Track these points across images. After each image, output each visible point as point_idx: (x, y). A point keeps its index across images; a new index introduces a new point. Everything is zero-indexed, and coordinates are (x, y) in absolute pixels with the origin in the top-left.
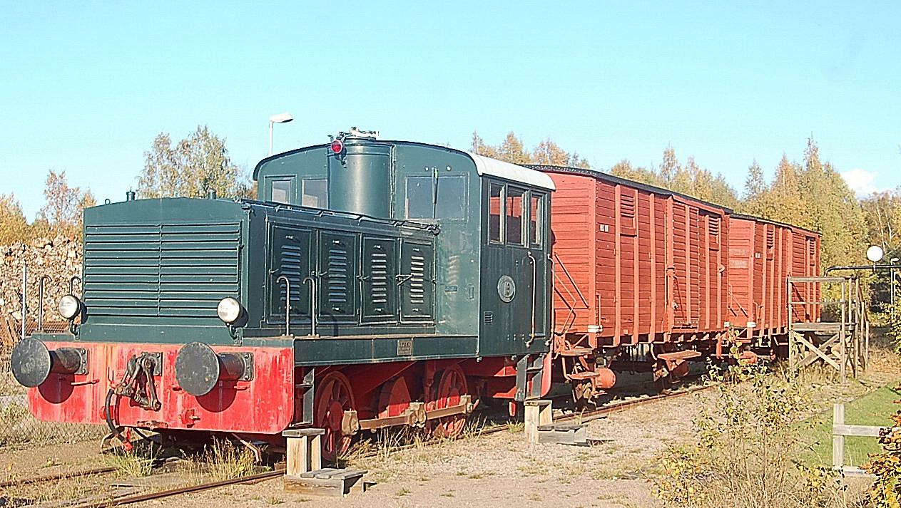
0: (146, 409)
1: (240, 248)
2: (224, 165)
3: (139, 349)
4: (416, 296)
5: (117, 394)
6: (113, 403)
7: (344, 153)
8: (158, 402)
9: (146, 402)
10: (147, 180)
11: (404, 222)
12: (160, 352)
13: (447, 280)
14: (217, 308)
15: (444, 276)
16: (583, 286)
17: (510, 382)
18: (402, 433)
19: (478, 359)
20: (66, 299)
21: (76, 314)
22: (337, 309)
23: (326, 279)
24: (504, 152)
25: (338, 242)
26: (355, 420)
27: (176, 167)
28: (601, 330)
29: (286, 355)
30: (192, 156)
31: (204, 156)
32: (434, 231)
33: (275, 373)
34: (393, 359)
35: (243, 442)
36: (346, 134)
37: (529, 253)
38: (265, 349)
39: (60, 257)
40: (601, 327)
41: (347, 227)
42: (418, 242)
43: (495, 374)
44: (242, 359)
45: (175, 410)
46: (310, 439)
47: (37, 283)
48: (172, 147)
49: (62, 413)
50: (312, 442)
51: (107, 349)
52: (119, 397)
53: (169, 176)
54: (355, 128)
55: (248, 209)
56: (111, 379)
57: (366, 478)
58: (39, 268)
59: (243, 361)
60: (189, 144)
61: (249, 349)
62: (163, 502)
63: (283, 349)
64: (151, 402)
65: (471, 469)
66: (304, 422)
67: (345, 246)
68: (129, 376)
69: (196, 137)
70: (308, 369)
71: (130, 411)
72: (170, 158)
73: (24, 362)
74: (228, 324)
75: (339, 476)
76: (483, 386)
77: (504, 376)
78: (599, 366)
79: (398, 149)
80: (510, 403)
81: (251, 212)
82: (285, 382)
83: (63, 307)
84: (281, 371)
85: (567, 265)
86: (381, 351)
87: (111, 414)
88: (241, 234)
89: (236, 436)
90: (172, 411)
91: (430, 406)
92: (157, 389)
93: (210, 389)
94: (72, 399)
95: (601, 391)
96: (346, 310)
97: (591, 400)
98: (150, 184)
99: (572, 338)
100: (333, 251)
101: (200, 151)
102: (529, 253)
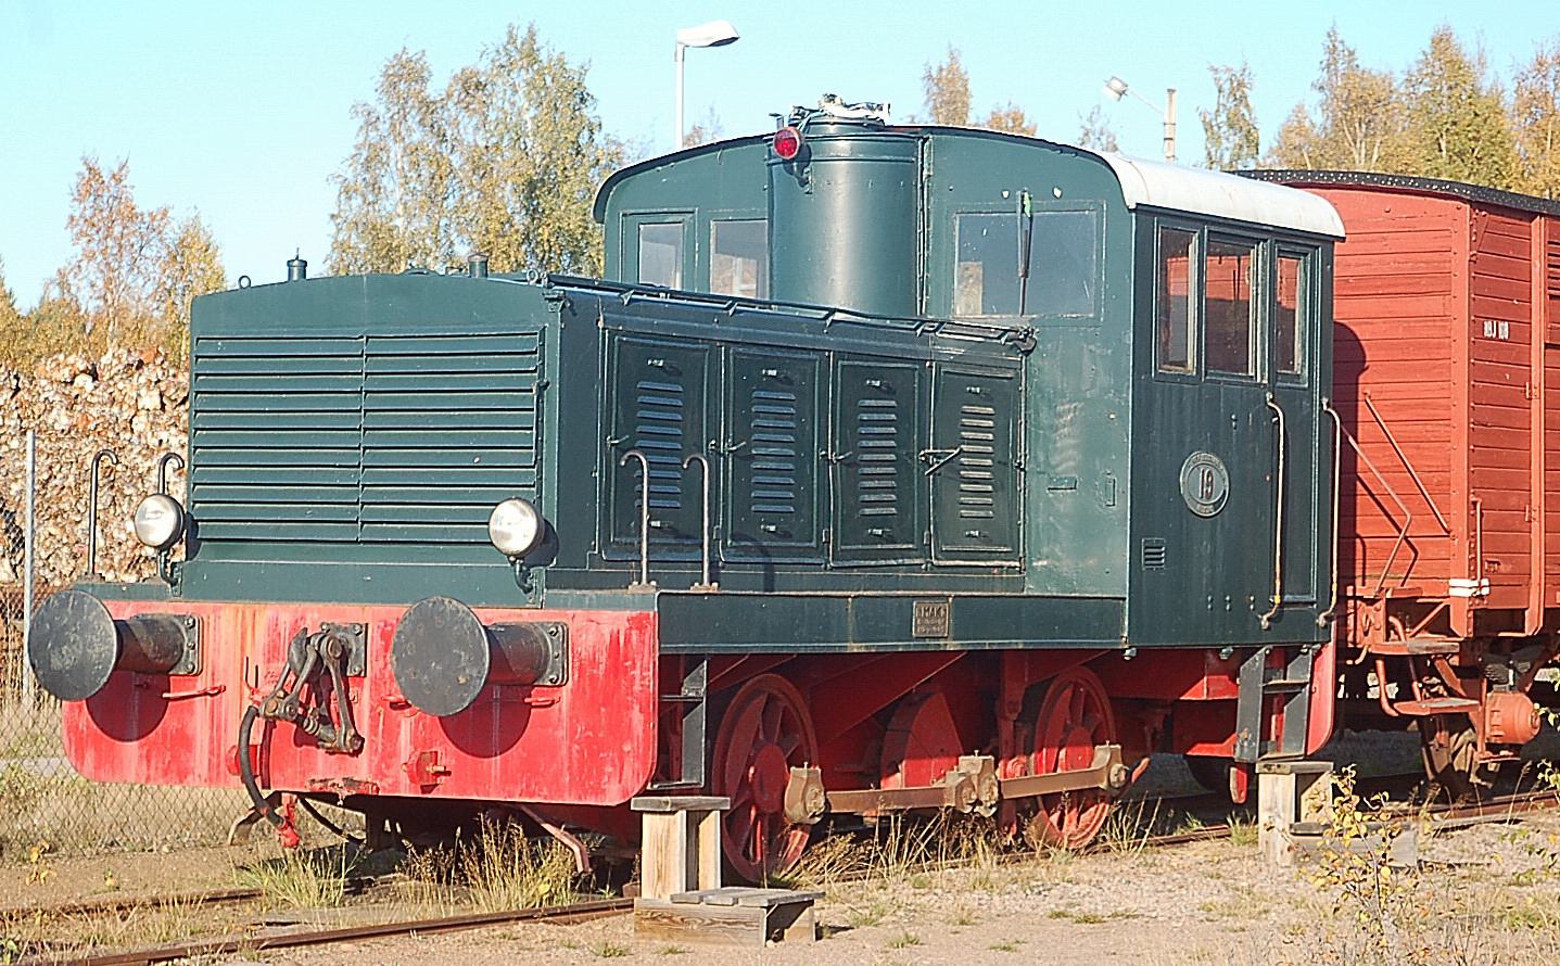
0: (331, 752)
1: (542, 388)
2: (583, 140)
3: (315, 615)
4: (972, 502)
5: (265, 716)
6: (257, 738)
7: (805, 157)
8: (357, 736)
9: (330, 735)
10: (361, 185)
11: (942, 323)
12: (363, 623)
13: (1053, 463)
14: (487, 524)
15: (1046, 451)
16: (1437, 478)
17: (1220, 719)
18: (934, 825)
19: (1128, 652)
20: (152, 504)
21: (175, 537)
22: (773, 528)
23: (848, 465)
24: (1422, 89)
25: (774, 373)
26: (815, 788)
27: (445, 149)
28: (1485, 591)
29: (641, 628)
30: (492, 116)
31: (527, 116)
32: (1022, 344)
33: (617, 669)
34: (901, 646)
35: (547, 827)
36: (812, 111)
37: (1269, 396)
38: (594, 614)
39: (115, 409)
40: (1485, 582)
41: (806, 337)
42: (978, 372)
43: (1182, 694)
44: (542, 636)
45: (394, 754)
46: (694, 820)
47: (53, 482)
48: (435, 89)
49: (140, 764)
50: (701, 826)
51: (244, 617)
52: (271, 724)
53: (425, 173)
54: (832, 98)
55: (558, 299)
56: (253, 684)
57: (822, 912)
58: (58, 439)
59: (545, 641)
60: (483, 79)
61: (560, 616)
62: (363, 949)
63: (634, 614)
64: (340, 735)
65: (1094, 904)
66: (683, 781)
67: (791, 383)
68: (292, 677)
69: (504, 60)
70: (694, 661)
71: (294, 757)
72: (428, 121)
73: (59, 644)
74: (512, 559)
75: (756, 901)
76: (1158, 724)
77: (1204, 698)
78: (1495, 686)
79: (937, 148)
80: (1233, 770)
81: (564, 306)
82: (637, 688)
83: (144, 522)
84: (627, 664)
85: (1396, 427)
86: (872, 618)
87: (252, 765)
88: (542, 357)
89: (529, 812)
90: (388, 755)
91: (1013, 766)
92: (355, 708)
93: (469, 700)
94: (164, 730)
95: (1503, 753)
96: (793, 532)
97: (1478, 774)
98: (371, 198)
99: (1407, 609)
100: (762, 394)
101: (514, 101)
102: (1269, 396)
